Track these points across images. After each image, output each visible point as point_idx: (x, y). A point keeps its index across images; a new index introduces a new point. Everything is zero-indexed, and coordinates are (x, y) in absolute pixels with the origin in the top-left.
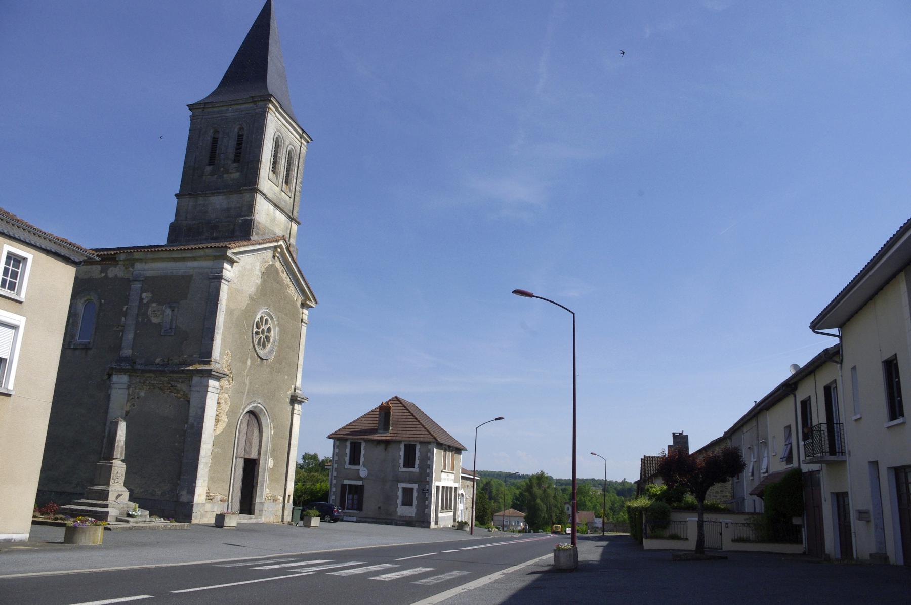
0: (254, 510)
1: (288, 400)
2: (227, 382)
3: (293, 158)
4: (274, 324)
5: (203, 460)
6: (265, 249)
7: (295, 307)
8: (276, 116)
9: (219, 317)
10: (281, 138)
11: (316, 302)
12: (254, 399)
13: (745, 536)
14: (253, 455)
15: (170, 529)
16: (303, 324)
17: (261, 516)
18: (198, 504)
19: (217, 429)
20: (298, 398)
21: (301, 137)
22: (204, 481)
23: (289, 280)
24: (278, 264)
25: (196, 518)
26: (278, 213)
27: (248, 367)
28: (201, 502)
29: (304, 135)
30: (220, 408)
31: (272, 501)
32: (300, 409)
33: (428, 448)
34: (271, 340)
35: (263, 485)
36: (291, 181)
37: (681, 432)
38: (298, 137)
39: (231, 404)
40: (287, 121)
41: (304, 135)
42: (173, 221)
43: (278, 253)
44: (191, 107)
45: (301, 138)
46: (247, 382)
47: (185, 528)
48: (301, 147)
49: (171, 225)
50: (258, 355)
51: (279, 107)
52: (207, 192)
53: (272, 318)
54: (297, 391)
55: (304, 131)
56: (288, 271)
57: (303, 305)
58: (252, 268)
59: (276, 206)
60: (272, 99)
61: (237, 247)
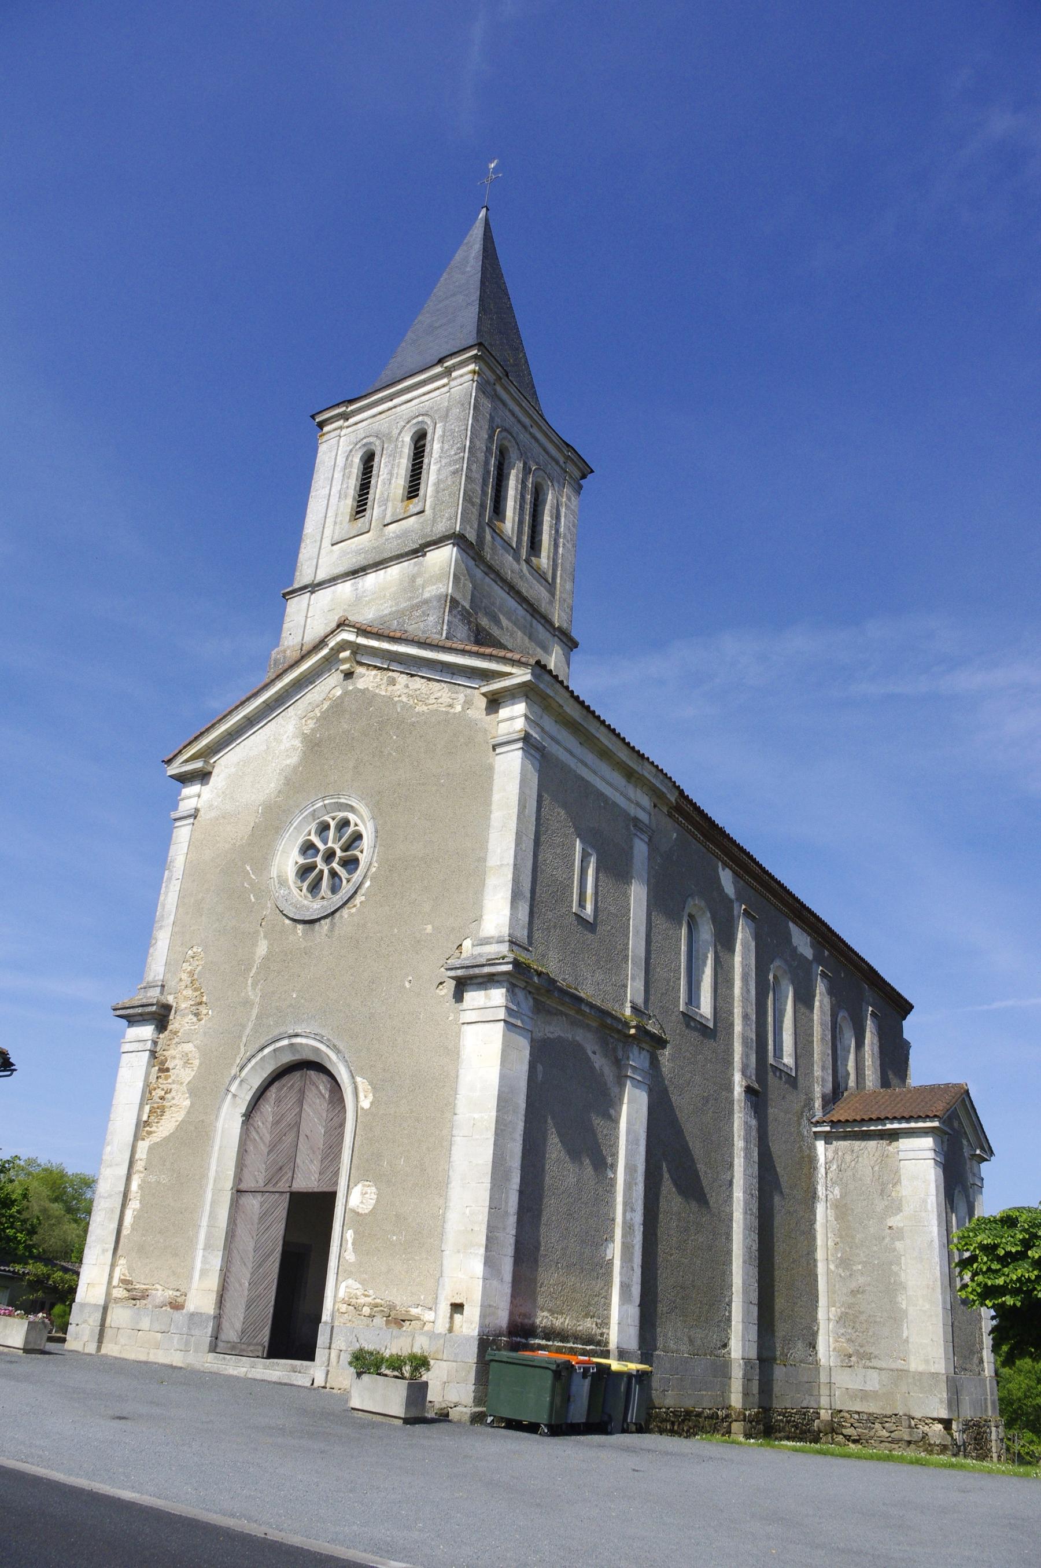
2: (191, 1016)
5: (102, 1204)
6: (447, 545)
7: (472, 724)
14: (307, 1181)
18: (83, 1305)
19: (161, 1128)
22: (104, 1251)
24: (368, 679)
25: (76, 1339)
27: (258, 961)
28: (92, 1301)
30: (170, 1081)
31: (379, 1321)
33: (1029, 1257)
34: (281, 1533)
37: (343, 675)
40: (390, 398)
42: (904, 1037)
49: (905, 1019)
52: (337, 527)
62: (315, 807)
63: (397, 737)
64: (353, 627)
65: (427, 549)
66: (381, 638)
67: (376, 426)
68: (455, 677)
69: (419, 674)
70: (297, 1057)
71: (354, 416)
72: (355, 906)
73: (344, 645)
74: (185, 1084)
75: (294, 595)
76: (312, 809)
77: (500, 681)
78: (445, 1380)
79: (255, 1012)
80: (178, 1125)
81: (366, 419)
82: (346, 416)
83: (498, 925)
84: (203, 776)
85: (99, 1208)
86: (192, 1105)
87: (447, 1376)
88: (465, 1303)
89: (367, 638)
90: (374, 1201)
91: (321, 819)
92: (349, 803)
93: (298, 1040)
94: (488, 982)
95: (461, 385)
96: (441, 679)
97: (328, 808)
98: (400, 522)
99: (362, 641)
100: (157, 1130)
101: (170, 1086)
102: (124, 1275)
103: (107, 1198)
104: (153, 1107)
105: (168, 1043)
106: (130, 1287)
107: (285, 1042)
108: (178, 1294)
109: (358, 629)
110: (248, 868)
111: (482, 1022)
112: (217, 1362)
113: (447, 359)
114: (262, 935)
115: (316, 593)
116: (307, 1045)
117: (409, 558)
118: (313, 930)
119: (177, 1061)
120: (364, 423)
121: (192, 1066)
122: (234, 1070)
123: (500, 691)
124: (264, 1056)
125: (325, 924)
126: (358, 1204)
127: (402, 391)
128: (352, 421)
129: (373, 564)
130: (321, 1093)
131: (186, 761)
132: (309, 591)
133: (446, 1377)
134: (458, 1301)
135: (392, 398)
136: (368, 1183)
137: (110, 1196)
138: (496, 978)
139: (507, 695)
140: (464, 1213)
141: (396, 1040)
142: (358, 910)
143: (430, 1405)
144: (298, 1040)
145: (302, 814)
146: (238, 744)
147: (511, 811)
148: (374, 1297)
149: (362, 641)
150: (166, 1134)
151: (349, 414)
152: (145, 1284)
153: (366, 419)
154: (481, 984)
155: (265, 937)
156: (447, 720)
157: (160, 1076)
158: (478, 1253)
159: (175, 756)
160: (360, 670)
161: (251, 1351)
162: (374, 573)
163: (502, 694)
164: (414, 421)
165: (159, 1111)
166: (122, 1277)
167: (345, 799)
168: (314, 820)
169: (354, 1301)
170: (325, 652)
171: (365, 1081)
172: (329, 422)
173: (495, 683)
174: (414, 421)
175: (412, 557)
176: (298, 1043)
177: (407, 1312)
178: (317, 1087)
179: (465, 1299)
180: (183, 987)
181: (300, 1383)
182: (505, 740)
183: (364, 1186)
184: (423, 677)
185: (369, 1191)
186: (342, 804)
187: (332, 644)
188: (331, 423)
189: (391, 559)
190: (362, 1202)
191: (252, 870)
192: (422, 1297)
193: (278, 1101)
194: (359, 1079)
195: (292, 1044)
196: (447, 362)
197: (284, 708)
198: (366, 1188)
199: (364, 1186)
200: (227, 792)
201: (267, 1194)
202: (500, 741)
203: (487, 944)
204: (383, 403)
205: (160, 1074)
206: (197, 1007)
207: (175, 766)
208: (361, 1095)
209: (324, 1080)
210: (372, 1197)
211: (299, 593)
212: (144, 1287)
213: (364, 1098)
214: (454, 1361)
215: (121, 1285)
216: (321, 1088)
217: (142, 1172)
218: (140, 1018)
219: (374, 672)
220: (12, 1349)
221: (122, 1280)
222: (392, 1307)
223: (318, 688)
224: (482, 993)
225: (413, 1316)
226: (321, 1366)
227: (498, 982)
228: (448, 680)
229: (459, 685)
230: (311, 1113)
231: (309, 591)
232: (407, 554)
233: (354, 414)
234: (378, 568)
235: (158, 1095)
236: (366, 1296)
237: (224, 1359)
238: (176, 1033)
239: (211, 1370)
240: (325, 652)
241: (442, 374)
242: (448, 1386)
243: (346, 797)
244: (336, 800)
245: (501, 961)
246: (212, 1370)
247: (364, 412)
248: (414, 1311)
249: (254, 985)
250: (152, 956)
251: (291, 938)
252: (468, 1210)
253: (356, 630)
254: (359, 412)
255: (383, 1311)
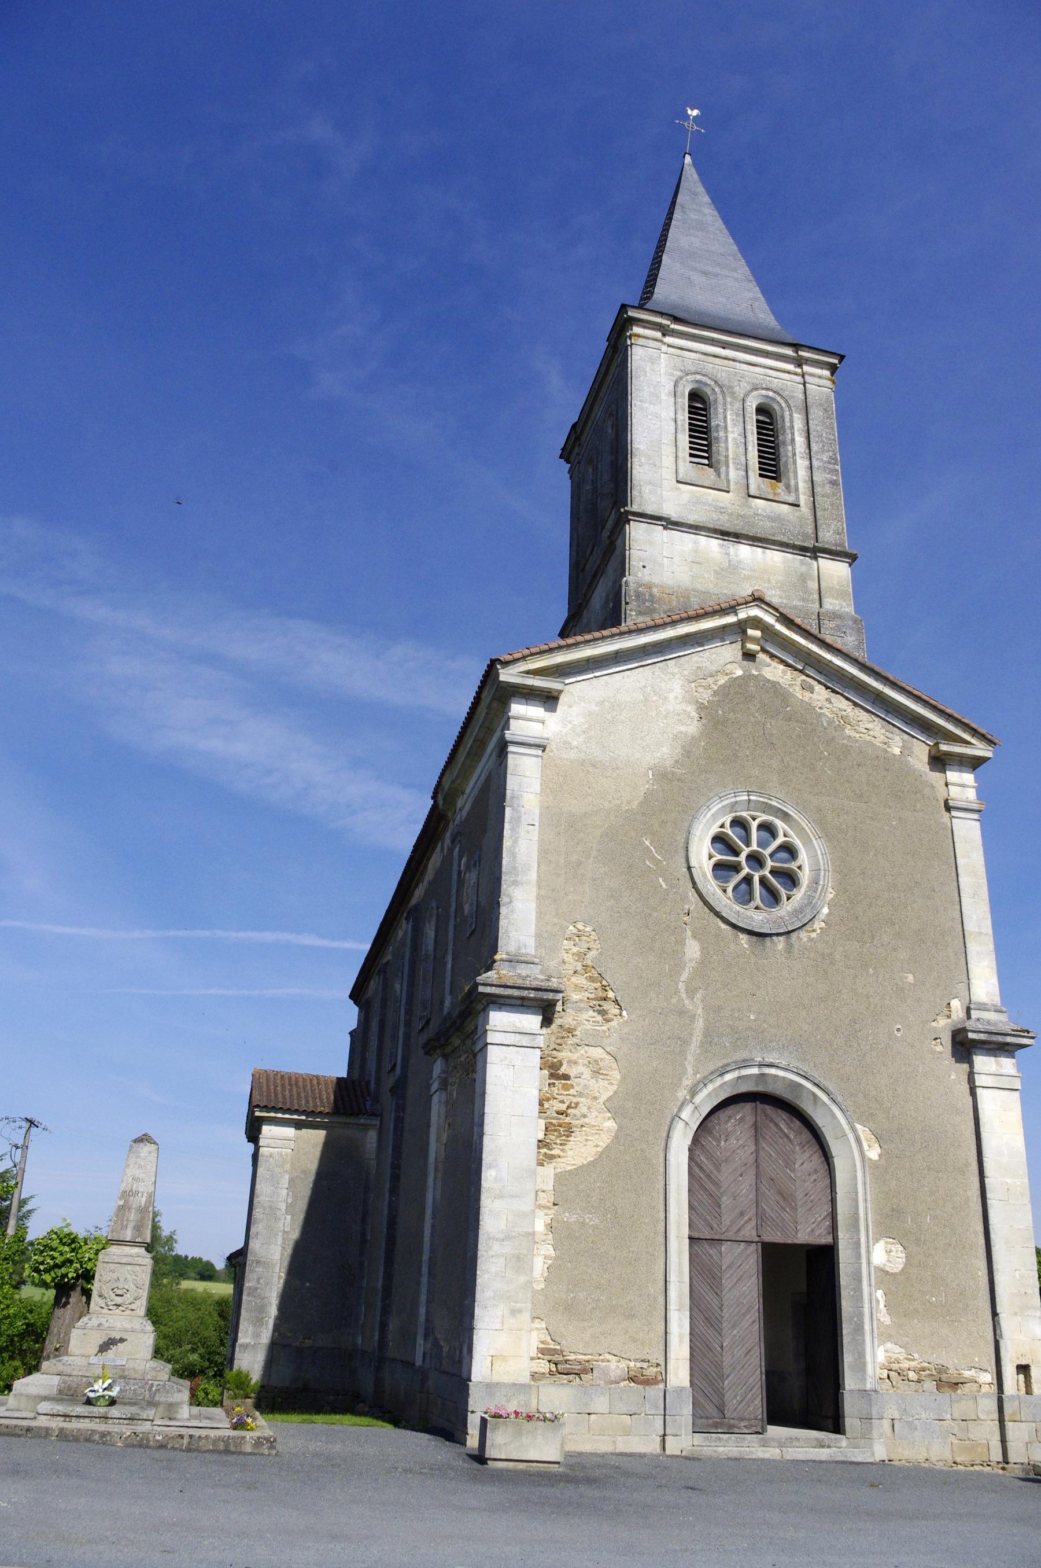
0: (844, 1417)
1: (944, 1048)
3: (782, 417)
4: (801, 832)
8: (669, 346)
9: (515, 842)
10: (706, 384)
11: (990, 742)
12: (744, 1054)
13: (807, 1155)
15: (162, 1446)
16: (954, 813)
17: (866, 1436)
19: (570, 1153)
20: (971, 1035)
21: (799, 362)
23: (844, 704)
24: (774, 671)
26: (744, 552)
29: (801, 353)
30: (572, 1091)
31: (930, 1385)
32: (1013, 1071)
34: (805, 877)
35: (859, 1329)
36: (791, 466)
38: (790, 367)
39: (624, 1078)
40: (724, 345)
41: (801, 353)
43: (754, 640)
44: (561, 457)
45: (800, 366)
46: (696, 1006)
47: (248, 1449)
48: (804, 384)
50: (734, 926)
51: (668, 322)
53: (785, 817)
54: (974, 1014)
55: (796, 346)
56: (831, 680)
57: (939, 762)
58: (646, 700)
59: (724, 534)
60: (630, 314)
61: (532, 654)
62: (738, 799)
63: (829, 754)
64: (776, 610)
65: (821, 555)
66: (811, 637)
67: (709, 368)
68: (890, 715)
69: (845, 694)
70: (761, 1088)
71: (672, 336)
72: (814, 931)
73: (756, 623)
74: (601, 1100)
75: (641, 519)
76: (734, 800)
77: (961, 746)
78: (1027, 1441)
79: (700, 1024)
80: (602, 1153)
81: (696, 352)
82: (665, 331)
83: (988, 993)
84: (549, 699)
85: (491, 1253)
86: (621, 1128)
87: (1029, 1436)
88: (1031, 1364)
89: (789, 629)
90: (904, 1260)
91: (738, 814)
92: (785, 809)
93: (773, 1071)
94: (997, 1049)
95: (819, 386)
96: (874, 711)
97: (752, 804)
98: (769, 503)
99: (779, 627)
100: (562, 1154)
101: (575, 1100)
102: (542, 1342)
103: (503, 1240)
104: (551, 1123)
105: (559, 1041)
106: (556, 1358)
107: (755, 1071)
108: (645, 1365)
109: (781, 613)
110: (647, 843)
111: (996, 1088)
112: (708, 1444)
113: (804, 349)
114: (689, 933)
115: (668, 531)
116: (784, 1078)
117: (794, 552)
118: (763, 945)
119: (580, 1068)
120: (693, 355)
121: (608, 1077)
122: (682, 1094)
123: (953, 754)
124: (725, 1083)
125: (780, 943)
126: (884, 1262)
127: (701, 338)
128: (668, 340)
129: (752, 537)
130: (782, 1131)
131: (528, 672)
132: (662, 525)
133: (1027, 1437)
134: (1024, 1363)
135: (725, 346)
136: (891, 1240)
137: (508, 1238)
138: (1007, 1048)
139: (954, 760)
140: (1014, 1277)
141: (896, 1090)
142: (820, 935)
143: (683, 1452)
144: (773, 1071)
145: (722, 801)
146: (596, 677)
147: (979, 881)
148: (920, 1361)
149: (779, 627)
150: (580, 1161)
151: (668, 331)
152: (585, 1355)
153: (696, 352)
154: (990, 1049)
155: (694, 937)
156: (884, 760)
157: (554, 1084)
158: (1035, 1316)
159: (515, 661)
160: (761, 656)
161: (745, 1426)
162: (749, 547)
163: (953, 757)
164: (771, 394)
165: (561, 1129)
166: (542, 1346)
167: (778, 802)
168: (731, 812)
169: (895, 1366)
170: (731, 619)
171: (866, 1129)
172: (641, 324)
173: (957, 746)
174: (771, 394)
175: (798, 552)
176: (772, 1075)
177: (960, 1374)
178: (777, 1125)
179: (1030, 1361)
180: (571, 972)
181: (859, 1459)
182: (965, 807)
183: (887, 1243)
184: (847, 699)
185: (894, 1250)
186: (771, 807)
187: (742, 615)
188: (644, 327)
189: (774, 543)
190: (889, 1261)
191: (655, 848)
192: (976, 1359)
193: (440, 1096)
194: (859, 1127)
195: (763, 1075)
196: (804, 351)
197: (662, 658)
198: (889, 1246)
199: (887, 1243)
200: (592, 733)
201: (729, 1243)
202: (959, 806)
203: (985, 1010)
204: (712, 345)
205: (552, 1081)
206: (601, 1003)
207: (511, 672)
208: (866, 1147)
209: (784, 1117)
210: (899, 1256)
211: (649, 521)
212: (586, 1358)
213: (868, 1148)
214: (1033, 1422)
215: (540, 1355)
216: (782, 1126)
217: (549, 1208)
218: (519, 1002)
219: (781, 667)
220: (535, 1464)
221: (542, 1349)
222: (942, 1369)
223: (707, 653)
224: (992, 1059)
225: (967, 1378)
226: (880, 1438)
227: (1007, 1051)
228: (884, 717)
229: (894, 725)
230: (773, 1154)
231: (662, 525)
232: (794, 547)
233: (674, 334)
234: (755, 544)
235: (555, 1108)
236: (909, 1360)
237: (719, 1439)
238: (570, 1031)
239: (729, 1456)
240: (731, 619)
241: (790, 358)
242: (1031, 1446)
243: (780, 801)
244: (766, 800)
245: (1026, 1034)
246: (731, 1455)
247: (687, 339)
248: (968, 1374)
249: (691, 993)
250: (506, 918)
251: (732, 947)
252: (1017, 1274)
253: (778, 615)
254: (680, 336)
255: (932, 1375)
